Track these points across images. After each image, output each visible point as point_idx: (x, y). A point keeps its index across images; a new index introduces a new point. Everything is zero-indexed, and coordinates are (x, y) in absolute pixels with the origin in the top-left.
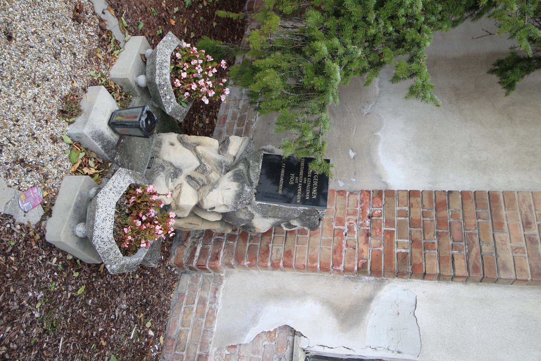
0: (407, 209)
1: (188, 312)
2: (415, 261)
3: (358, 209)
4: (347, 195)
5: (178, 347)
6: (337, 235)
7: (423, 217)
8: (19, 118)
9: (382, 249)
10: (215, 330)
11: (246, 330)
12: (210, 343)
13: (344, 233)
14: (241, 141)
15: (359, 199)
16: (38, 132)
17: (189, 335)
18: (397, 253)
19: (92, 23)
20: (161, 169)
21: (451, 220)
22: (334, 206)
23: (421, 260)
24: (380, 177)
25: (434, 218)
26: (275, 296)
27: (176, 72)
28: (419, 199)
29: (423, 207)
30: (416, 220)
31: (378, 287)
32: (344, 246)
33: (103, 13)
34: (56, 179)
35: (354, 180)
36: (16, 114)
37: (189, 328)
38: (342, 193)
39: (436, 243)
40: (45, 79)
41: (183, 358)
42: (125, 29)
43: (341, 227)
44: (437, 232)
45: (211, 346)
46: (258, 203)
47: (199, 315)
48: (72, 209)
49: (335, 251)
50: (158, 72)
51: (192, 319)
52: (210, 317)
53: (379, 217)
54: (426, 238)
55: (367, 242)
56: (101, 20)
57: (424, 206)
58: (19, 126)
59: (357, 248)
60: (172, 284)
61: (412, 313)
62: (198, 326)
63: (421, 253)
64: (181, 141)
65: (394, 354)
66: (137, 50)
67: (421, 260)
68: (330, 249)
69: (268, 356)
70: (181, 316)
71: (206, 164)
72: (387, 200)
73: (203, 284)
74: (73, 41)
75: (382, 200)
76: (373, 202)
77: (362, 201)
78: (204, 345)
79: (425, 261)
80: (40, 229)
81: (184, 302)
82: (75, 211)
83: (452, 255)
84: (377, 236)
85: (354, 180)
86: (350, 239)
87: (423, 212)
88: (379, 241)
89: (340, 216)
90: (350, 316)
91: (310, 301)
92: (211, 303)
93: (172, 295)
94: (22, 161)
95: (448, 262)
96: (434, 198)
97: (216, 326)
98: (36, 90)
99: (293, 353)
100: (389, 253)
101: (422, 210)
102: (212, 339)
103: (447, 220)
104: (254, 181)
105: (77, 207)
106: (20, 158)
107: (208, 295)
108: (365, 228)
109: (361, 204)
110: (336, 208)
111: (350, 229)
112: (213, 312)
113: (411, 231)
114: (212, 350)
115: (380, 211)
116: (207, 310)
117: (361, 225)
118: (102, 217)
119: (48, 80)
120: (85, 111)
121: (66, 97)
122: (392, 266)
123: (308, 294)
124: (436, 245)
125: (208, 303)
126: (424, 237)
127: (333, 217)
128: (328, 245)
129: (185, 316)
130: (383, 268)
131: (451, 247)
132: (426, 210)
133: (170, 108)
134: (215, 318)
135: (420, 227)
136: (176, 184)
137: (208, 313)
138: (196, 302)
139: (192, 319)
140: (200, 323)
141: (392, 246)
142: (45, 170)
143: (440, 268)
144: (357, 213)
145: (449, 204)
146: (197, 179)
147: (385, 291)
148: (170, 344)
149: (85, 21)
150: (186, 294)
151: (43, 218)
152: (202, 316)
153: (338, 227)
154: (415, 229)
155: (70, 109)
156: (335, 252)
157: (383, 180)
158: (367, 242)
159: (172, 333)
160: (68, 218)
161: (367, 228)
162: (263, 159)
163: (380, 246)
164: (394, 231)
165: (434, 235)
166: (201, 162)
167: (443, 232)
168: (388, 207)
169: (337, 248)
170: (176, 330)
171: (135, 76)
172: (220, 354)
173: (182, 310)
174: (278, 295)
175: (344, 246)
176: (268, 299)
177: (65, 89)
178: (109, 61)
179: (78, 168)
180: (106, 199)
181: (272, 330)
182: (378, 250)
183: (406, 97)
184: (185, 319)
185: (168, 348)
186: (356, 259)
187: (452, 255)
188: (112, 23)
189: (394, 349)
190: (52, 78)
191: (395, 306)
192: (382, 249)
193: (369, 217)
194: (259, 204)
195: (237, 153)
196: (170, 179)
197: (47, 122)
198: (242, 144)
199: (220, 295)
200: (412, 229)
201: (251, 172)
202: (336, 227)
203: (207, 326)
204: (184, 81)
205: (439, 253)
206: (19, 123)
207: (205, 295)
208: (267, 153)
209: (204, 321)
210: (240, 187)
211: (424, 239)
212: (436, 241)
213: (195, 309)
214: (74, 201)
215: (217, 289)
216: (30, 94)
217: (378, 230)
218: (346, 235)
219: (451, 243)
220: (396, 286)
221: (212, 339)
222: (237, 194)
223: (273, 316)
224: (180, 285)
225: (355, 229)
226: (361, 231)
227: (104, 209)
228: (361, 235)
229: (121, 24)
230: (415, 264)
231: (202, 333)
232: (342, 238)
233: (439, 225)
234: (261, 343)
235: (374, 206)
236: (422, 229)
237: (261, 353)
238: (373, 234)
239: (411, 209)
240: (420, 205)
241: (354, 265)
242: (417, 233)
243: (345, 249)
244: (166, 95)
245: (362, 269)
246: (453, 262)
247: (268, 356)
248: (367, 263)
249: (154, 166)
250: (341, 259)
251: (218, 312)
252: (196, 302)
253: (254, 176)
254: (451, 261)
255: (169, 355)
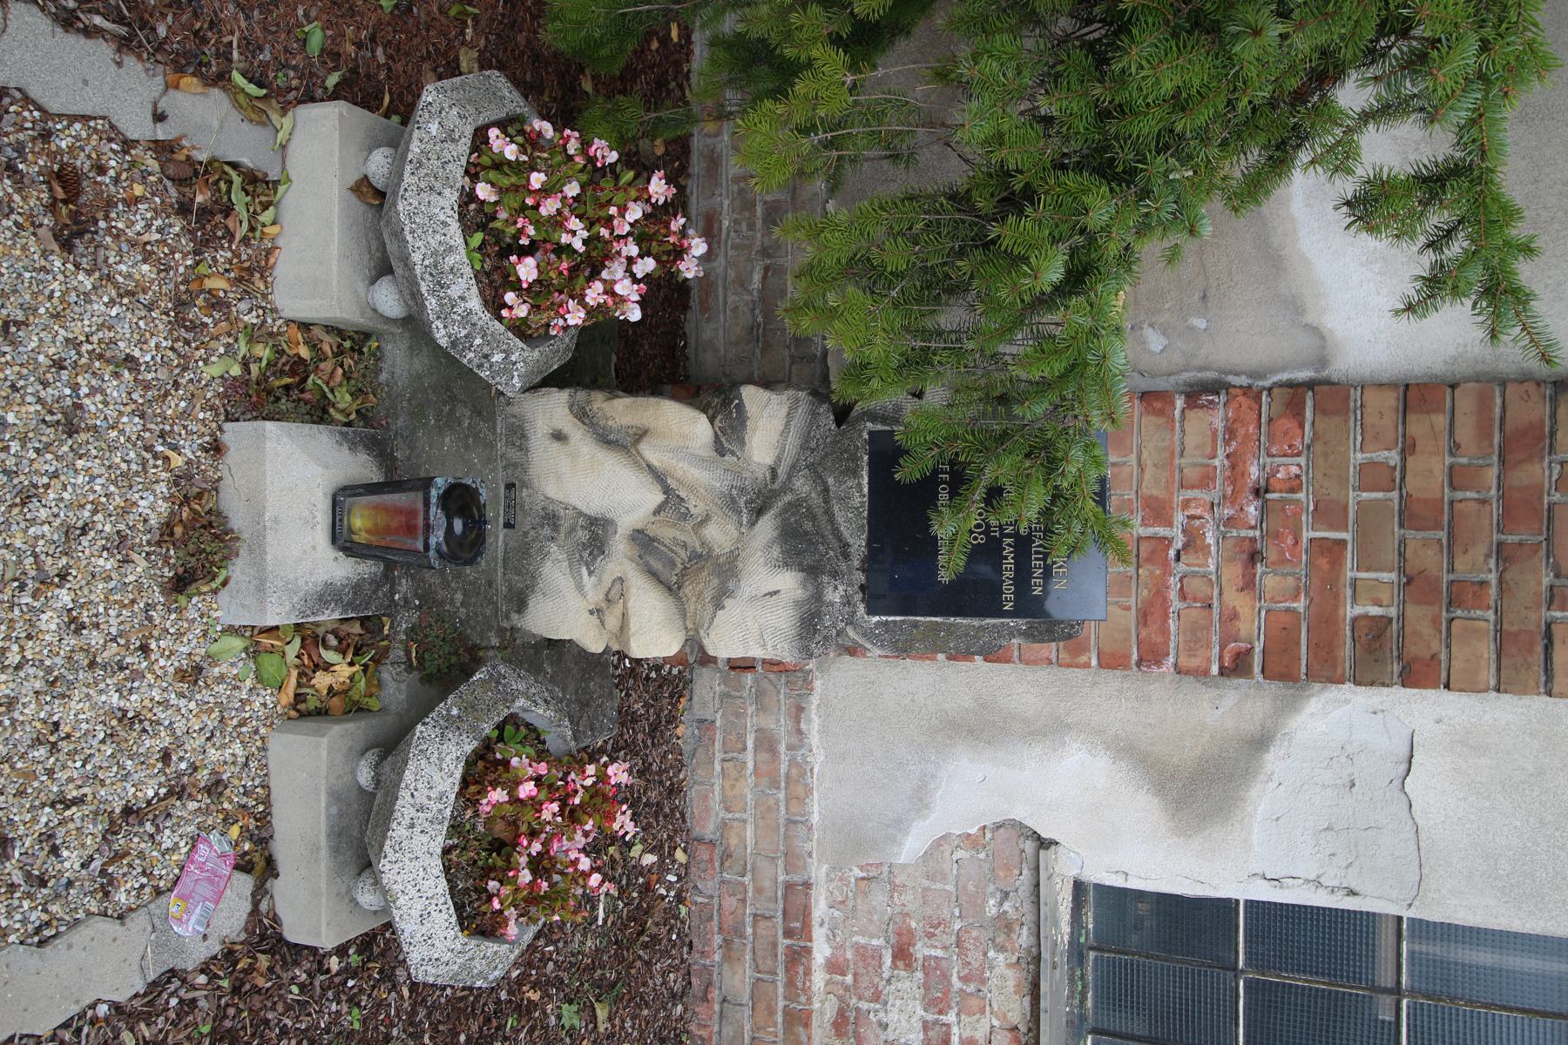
0: (1393, 457)
1: (734, 774)
2: (1413, 650)
3: (1217, 462)
4: (1177, 413)
5: (727, 864)
6: (1148, 560)
7: (1453, 487)
8: (55, 718)
9: (1300, 605)
10: (815, 819)
11: (900, 825)
12: (810, 855)
13: (1172, 553)
14: (785, 410)
15: (1220, 425)
16: (133, 698)
17: (749, 832)
18: (1355, 620)
19: (138, 190)
20: (547, 531)
21: (1557, 497)
22: (1133, 458)
23: (1436, 645)
24: (1295, 307)
25: (1493, 492)
26: (971, 732)
27: (496, 255)
28: (1441, 421)
29: (1454, 448)
30: (1426, 502)
31: (1290, 706)
32: (1173, 595)
33: (159, 117)
34: (246, 765)
35: (1200, 323)
36: (42, 715)
37: (745, 816)
38: (1158, 405)
39: (1494, 582)
40: (74, 533)
41: (746, 891)
42: (255, 112)
43: (1161, 531)
44: (1500, 544)
45: (814, 860)
46: (877, 618)
47: (764, 781)
48: (324, 853)
49: (1145, 616)
50: (432, 303)
51: (747, 791)
52: (797, 783)
53: (1292, 490)
54: (1457, 566)
55: (1249, 584)
56: (164, 149)
57: (1458, 446)
58: (68, 736)
59: (1216, 604)
60: (674, 706)
61: (1397, 783)
62: (769, 809)
63: (1436, 621)
64: (582, 415)
65: (1334, 898)
66: (336, 181)
67: (1436, 645)
68: (1128, 608)
69: (971, 888)
70: (718, 782)
71: (683, 494)
72: (1320, 426)
73: (759, 695)
74: (101, 327)
75: (1302, 426)
76: (1270, 437)
77: (1230, 432)
78: (793, 859)
79: (1449, 646)
80: (264, 934)
81: (718, 745)
82: (335, 850)
83: (1548, 626)
84: (1284, 561)
85: (1200, 323)
86: (1194, 574)
87: (1451, 468)
88: (1290, 580)
89: (1155, 492)
90: (1201, 789)
91: (1075, 746)
92: (790, 748)
93: (679, 731)
94: (128, 811)
95: (1531, 651)
96: (1498, 410)
97: (816, 809)
98: (65, 597)
99: (1038, 885)
100: (1325, 621)
101: (1448, 460)
102: (812, 846)
103: (1541, 498)
104: (851, 541)
105: (339, 835)
106: (118, 811)
107: (779, 725)
108: (1243, 533)
109: (1227, 442)
110: (1139, 464)
111: (1193, 541)
112: (803, 774)
113: (1403, 542)
114: (818, 871)
115: (1294, 470)
116: (783, 768)
117: (1230, 522)
118: (415, 913)
119: (84, 530)
120: (245, 536)
121: (167, 528)
122: (1335, 666)
123: (1068, 726)
124: (1493, 591)
125: (782, 748)
126: (1451, 563)
127: (1133, 496)
128: (1120, 594)
129: (727, 784)
130: (1303, 670)
131: (1545, 595)
132: (1464, 461)
133: (516, 380)
134: (809, 791)
135: (1437, 526)
136: (607, 580)
137: (788, 775)
138: (750, 744)
139: (747, 791)
140: (771, 801)
141: (1336, 596)
142: (203, 776)
143: (1499, 669)
144: (1213, 479)
145: (1553, 434)
146: (667, 541)
147: (1312, 715)
148: (706, 857)
149: (110, 204)
150: (718, 724)
151: (259, 892)
152: (775, 784)
153: (1150, 531)
154: (1422, 534)
155: (198, 546)
156: (1144, 617)
157: (1309, 318)
158: (1249, 584)
159: (703, 827)
160: (323, 886)
161: (1251, 533)
162: (871, 455)
163: (1295, 598)
164: (1343, 543)
165: (1488, 556)
166: (667, 490)
167: (1520, 544)
168: (1326, 455)
169: (1151, 604)
170: (713, 819)
171: (361, 287)
172: (841, 879)
173: (718, 767)
174: (981, 729)
175: (1173, 595)
176: (951, 738)
177: (153, 505)
178: (253, 272)
179: (299, 685)
180: (409, 866)
181: (973, 831)
182: (1287, 610)
183: (1410, 308)
184: (729, 793)
185: (702, 866)
186: (1215, 639)
187: (1548, 626)
188: (209, 121)
189: (1335, 883)
190: (95, 512)
191: (1343, 759)
192: (1300, 605)
193: (1257, 492)
194: (878, 624)
195: (779, 459)
196: (584, 571)
197: (144, 649)
198: (787, 425)
199: (813, 724)
200: (1410, 534)
201: (836, 508)
202: (1143, 532)
203: (793, 809)
204: (537, 293)
205: (1499, 621)
206: (65, 729)
207: (769, 722)
208: (879, 427)
209: (782, 796)
210: (810, 587)
211: (1451, 570)
212: (1493, 578)
213: (750, 765)
214: (323, 827)
215: (800, 709)
216: (49, 622)
217: (1290, 541)
218: (1178, 558)
219: (1546, 581)
220: (1347, 701)
221: (812, 846)
222: (802, 620)
223: (972, 792)
224: (695, 699)
225: (1210, 539)
226: (1229, 544)
227: (413, 892)
228: (1230, 560)
229: (241, 98)
230: (1415, 659)
231: (782, 830)
232: (1167, 572)
233: (1506, 520)
234: (947, 854)
235: (1274, 450)
236: (1443, 535)
237: (951, 879)
238: (1271, 554)
239: (1410, 459)
240: (1444, 442)
241: (1209, 660)
242: (1426, 553)
243: (1176, 604)
244: (486, 356)
245: (1237, 667)
246: (1548, 648)
247: (971, 888)
248: (1250, 651)
249: (525, 523)
250: (1166, 643)
251: (816, 770)
252: (750, 744)
253: (848, 521)
254: (1540, 649)
255: (710, 884)
